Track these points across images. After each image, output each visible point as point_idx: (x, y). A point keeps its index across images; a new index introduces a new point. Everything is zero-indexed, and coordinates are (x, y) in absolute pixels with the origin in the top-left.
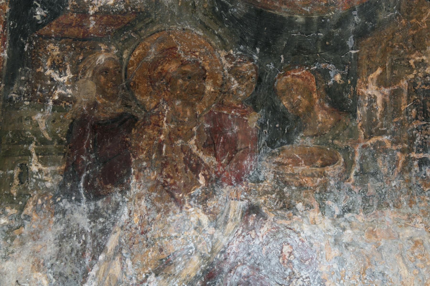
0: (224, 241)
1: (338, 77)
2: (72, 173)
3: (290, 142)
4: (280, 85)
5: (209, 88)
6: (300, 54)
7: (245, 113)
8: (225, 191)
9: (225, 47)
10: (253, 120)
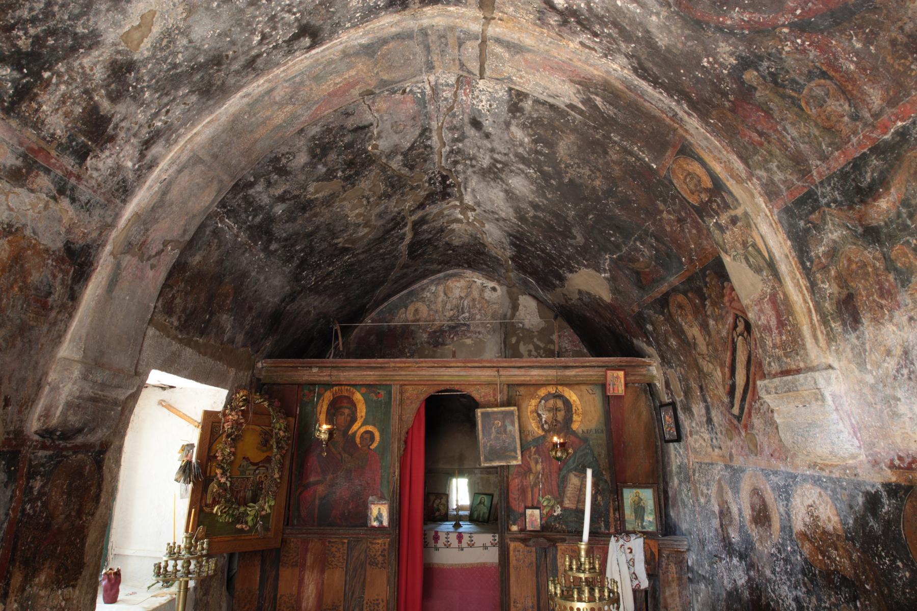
0: (906, 336)
1: (915, 241)
2: (844, 324)
3: (910, 282)
4: (893, 257)
5: (870, 270)
6: (892, 238)
7: (887, 276)
8: (897, 314)
9: (866, 249)
10: (891, 277)
